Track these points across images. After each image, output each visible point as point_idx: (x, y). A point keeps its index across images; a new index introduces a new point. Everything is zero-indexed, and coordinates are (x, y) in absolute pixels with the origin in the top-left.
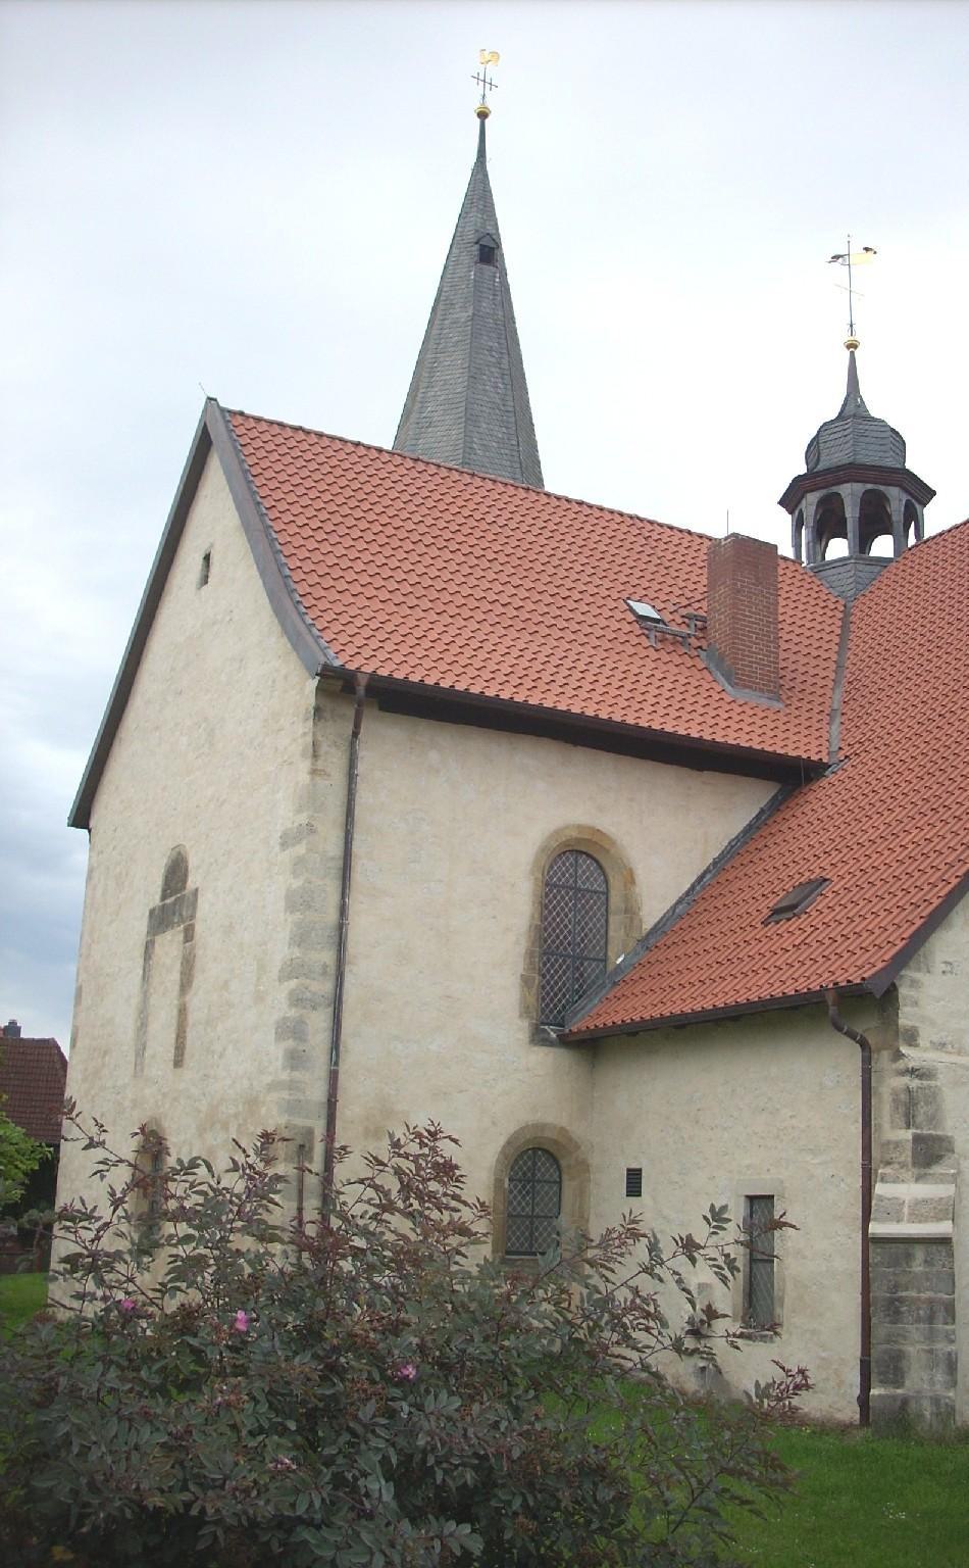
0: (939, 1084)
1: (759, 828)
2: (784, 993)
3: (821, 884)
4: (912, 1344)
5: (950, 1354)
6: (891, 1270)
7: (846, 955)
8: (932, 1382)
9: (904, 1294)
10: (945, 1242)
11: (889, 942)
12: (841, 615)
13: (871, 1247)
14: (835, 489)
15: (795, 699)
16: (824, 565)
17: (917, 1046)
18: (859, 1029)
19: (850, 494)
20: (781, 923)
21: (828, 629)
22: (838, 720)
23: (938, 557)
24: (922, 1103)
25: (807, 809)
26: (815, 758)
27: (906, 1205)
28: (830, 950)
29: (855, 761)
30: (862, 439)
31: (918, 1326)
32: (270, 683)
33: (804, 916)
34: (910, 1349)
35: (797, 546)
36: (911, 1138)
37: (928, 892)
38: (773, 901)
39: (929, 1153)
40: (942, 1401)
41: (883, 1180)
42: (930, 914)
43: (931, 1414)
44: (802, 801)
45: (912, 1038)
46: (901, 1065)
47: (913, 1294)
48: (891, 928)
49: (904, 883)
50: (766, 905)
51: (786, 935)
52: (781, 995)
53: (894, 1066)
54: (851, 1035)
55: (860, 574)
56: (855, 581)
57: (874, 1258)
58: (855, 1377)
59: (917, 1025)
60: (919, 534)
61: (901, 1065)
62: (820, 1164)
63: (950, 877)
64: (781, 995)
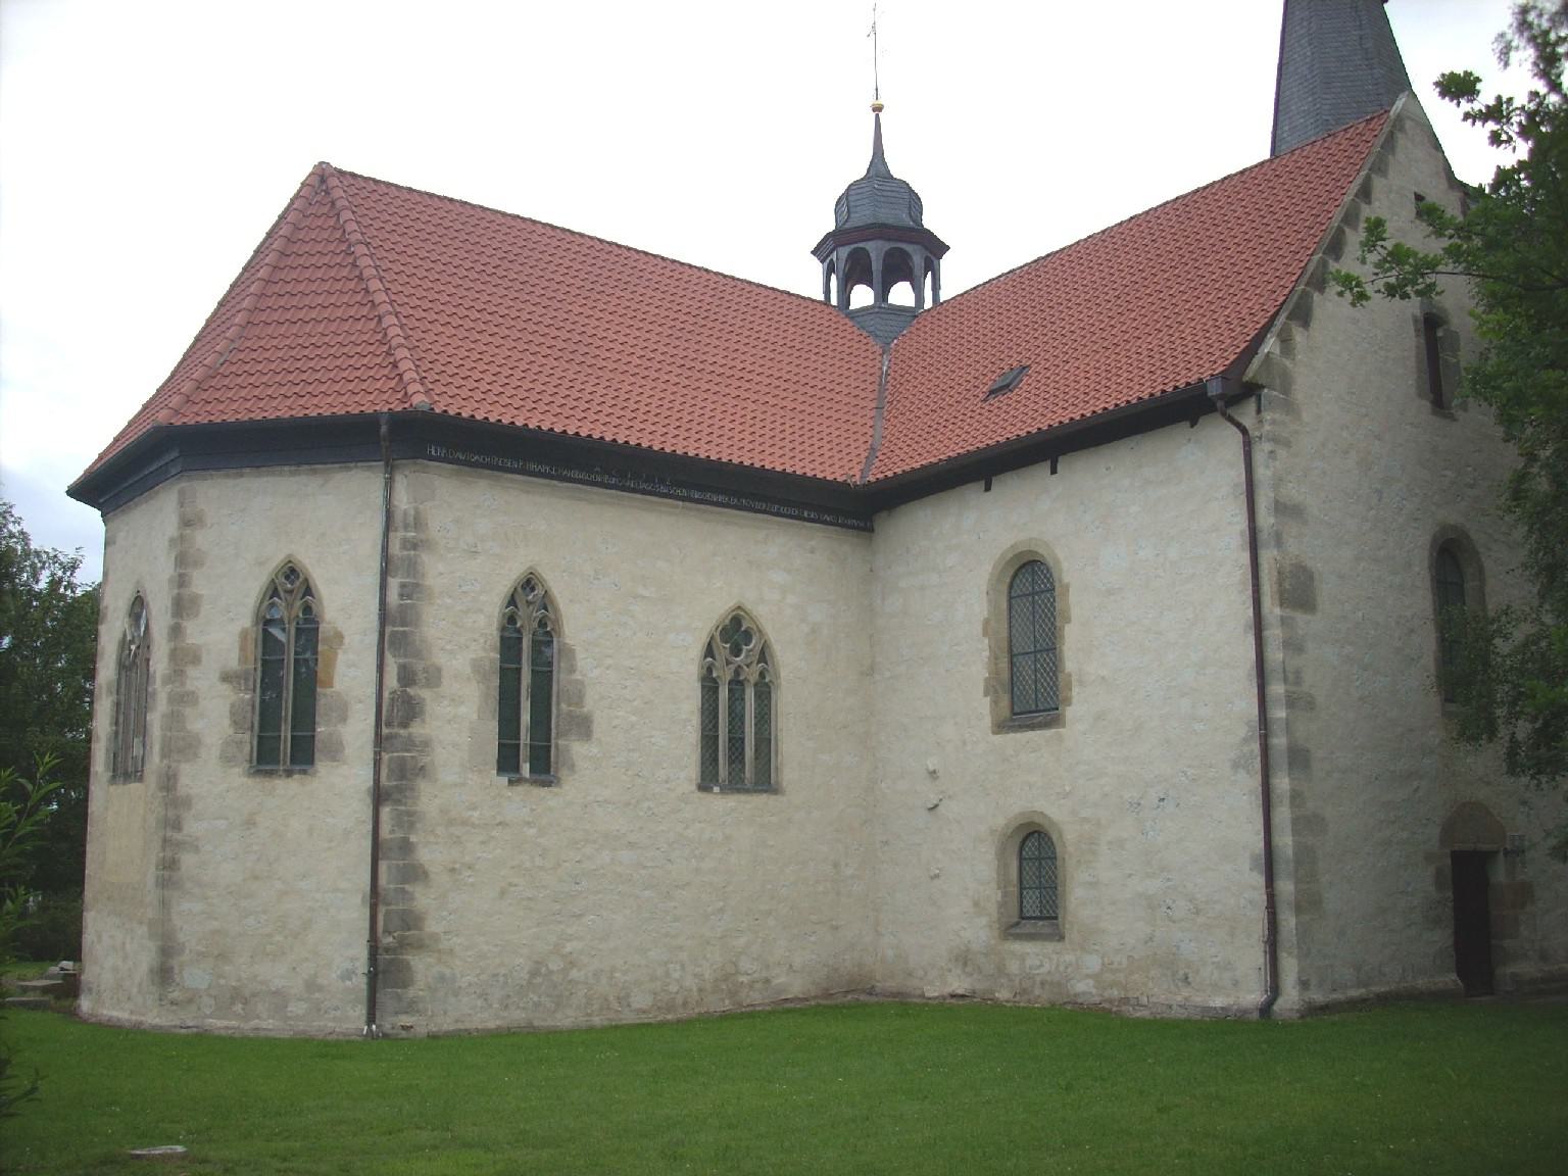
19: (876, 250)
32: (174, 1008)
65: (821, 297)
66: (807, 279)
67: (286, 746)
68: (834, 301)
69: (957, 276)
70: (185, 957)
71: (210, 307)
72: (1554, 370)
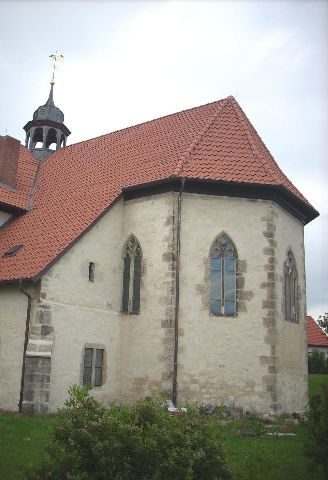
0: (51, 310)
1: (4, 228)
2: (6, 279)
3: (21, 247)
4: (36, 388)
5: (47, 391)
6: (32, 366)
7: (26, 269)
8: (41, 400)
9: (35, 373)
10: (48, 358)
11: (40, 267)
12: (37, 166)
13: (26, 359)
14: (41, 127)
15: (20, 189)
16: (34, 150)
17: (45, 299)
18: (28, 292)
19: (45, 129)
20: (11, 257)
21: (33, 169)
22: (33, 197)
23: (77, 148)
24: (45, 316)
25: (20, 223)
26: (24, 208)
27: (38, 347)
28: (22, 267)
29: (36, 210)
30: (51, 113)
31: (38, 383)
33: (15, 256)
34: (35, 390)
35: (27, 142)
36: (41, 326)
37: (54, 253)
38: (6, 251)
39: (46, 331)
40: (44, 406)
41: (31, 339)
42: (53, 259)
43: (41, 409)
44: (18, 221)
45: (44, 296)
46: (40, 304)
47: (37, 373)
48: (41, 262)
49: (43, 250)
50: (3, 252)
51: (9, 261)
52: (5, 280)
53: (38, 304)
54: (26, 294)
55: (45, 154)
56: (43, 156)
57: (27, 362)
58: (18, 398)
59: (46, 292)
60: (65, 144)
61: (40, 304)
62: (13, 332)
63: (61, 249)
64: (5, 280)
67: (130, 307)
71: (263, 140)
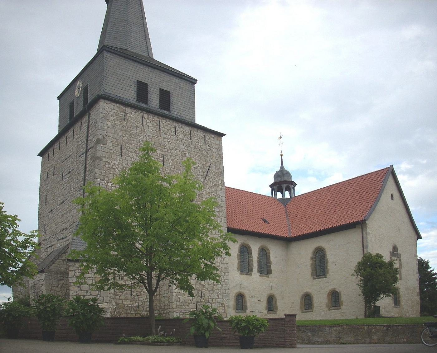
65: (271, 196)
66: (267, 192)
68: (274, 197)
69: (300, 190)
70: (329, 274)
72: (70, 259)
